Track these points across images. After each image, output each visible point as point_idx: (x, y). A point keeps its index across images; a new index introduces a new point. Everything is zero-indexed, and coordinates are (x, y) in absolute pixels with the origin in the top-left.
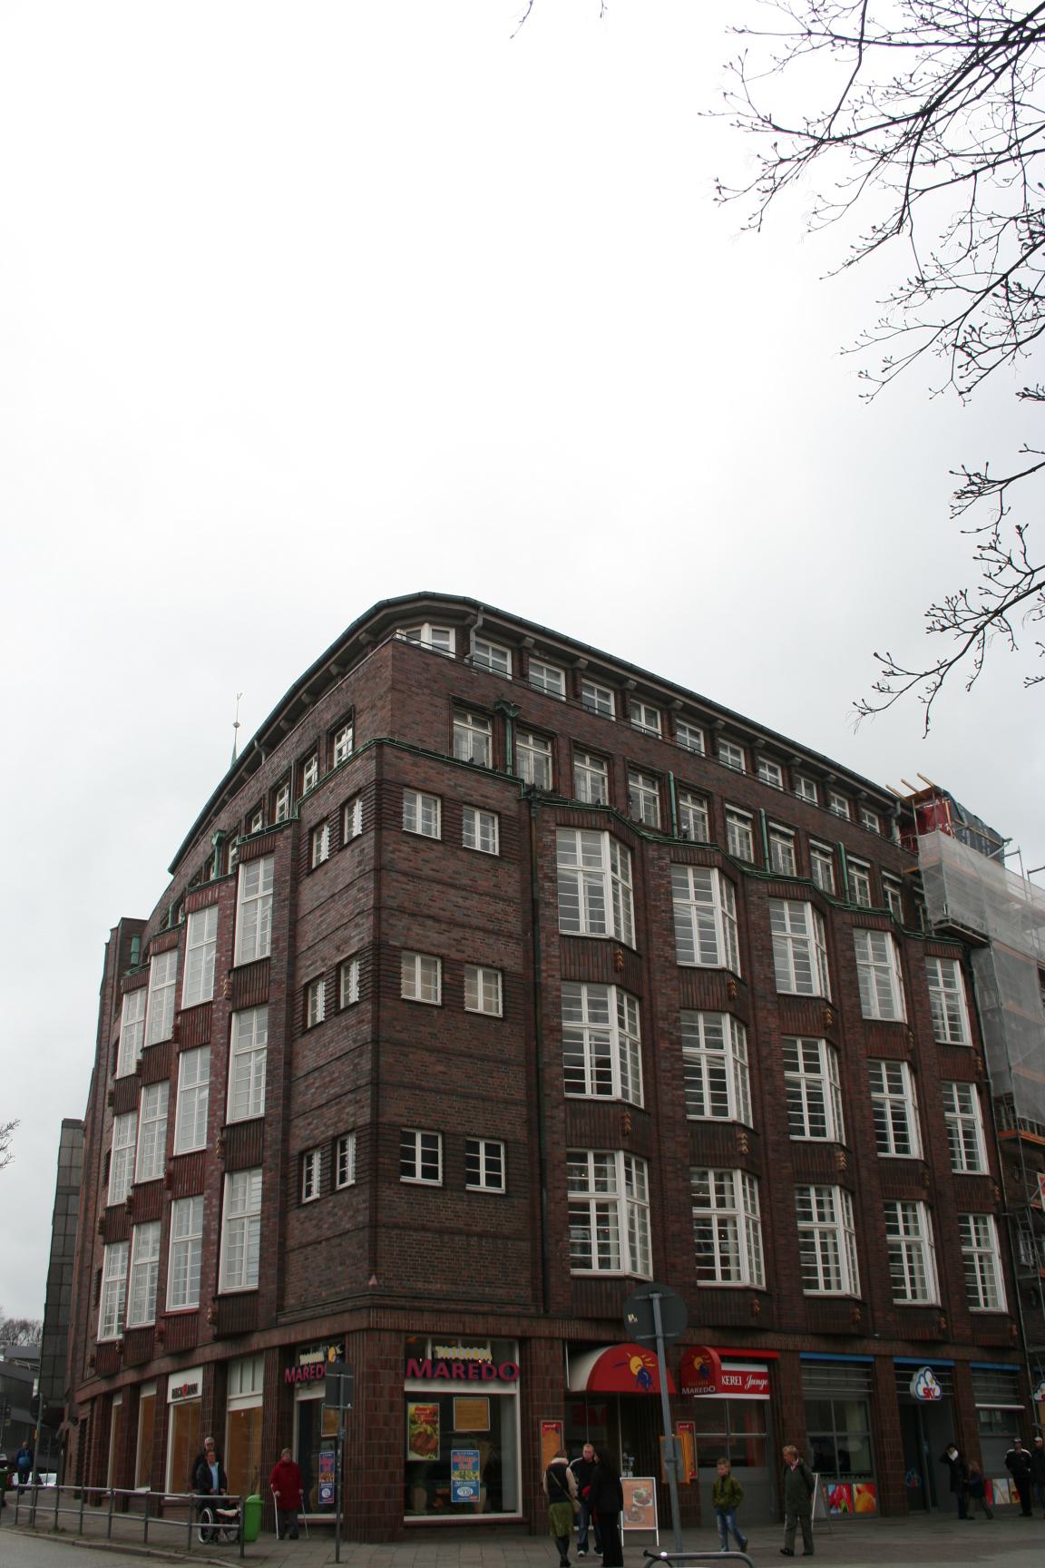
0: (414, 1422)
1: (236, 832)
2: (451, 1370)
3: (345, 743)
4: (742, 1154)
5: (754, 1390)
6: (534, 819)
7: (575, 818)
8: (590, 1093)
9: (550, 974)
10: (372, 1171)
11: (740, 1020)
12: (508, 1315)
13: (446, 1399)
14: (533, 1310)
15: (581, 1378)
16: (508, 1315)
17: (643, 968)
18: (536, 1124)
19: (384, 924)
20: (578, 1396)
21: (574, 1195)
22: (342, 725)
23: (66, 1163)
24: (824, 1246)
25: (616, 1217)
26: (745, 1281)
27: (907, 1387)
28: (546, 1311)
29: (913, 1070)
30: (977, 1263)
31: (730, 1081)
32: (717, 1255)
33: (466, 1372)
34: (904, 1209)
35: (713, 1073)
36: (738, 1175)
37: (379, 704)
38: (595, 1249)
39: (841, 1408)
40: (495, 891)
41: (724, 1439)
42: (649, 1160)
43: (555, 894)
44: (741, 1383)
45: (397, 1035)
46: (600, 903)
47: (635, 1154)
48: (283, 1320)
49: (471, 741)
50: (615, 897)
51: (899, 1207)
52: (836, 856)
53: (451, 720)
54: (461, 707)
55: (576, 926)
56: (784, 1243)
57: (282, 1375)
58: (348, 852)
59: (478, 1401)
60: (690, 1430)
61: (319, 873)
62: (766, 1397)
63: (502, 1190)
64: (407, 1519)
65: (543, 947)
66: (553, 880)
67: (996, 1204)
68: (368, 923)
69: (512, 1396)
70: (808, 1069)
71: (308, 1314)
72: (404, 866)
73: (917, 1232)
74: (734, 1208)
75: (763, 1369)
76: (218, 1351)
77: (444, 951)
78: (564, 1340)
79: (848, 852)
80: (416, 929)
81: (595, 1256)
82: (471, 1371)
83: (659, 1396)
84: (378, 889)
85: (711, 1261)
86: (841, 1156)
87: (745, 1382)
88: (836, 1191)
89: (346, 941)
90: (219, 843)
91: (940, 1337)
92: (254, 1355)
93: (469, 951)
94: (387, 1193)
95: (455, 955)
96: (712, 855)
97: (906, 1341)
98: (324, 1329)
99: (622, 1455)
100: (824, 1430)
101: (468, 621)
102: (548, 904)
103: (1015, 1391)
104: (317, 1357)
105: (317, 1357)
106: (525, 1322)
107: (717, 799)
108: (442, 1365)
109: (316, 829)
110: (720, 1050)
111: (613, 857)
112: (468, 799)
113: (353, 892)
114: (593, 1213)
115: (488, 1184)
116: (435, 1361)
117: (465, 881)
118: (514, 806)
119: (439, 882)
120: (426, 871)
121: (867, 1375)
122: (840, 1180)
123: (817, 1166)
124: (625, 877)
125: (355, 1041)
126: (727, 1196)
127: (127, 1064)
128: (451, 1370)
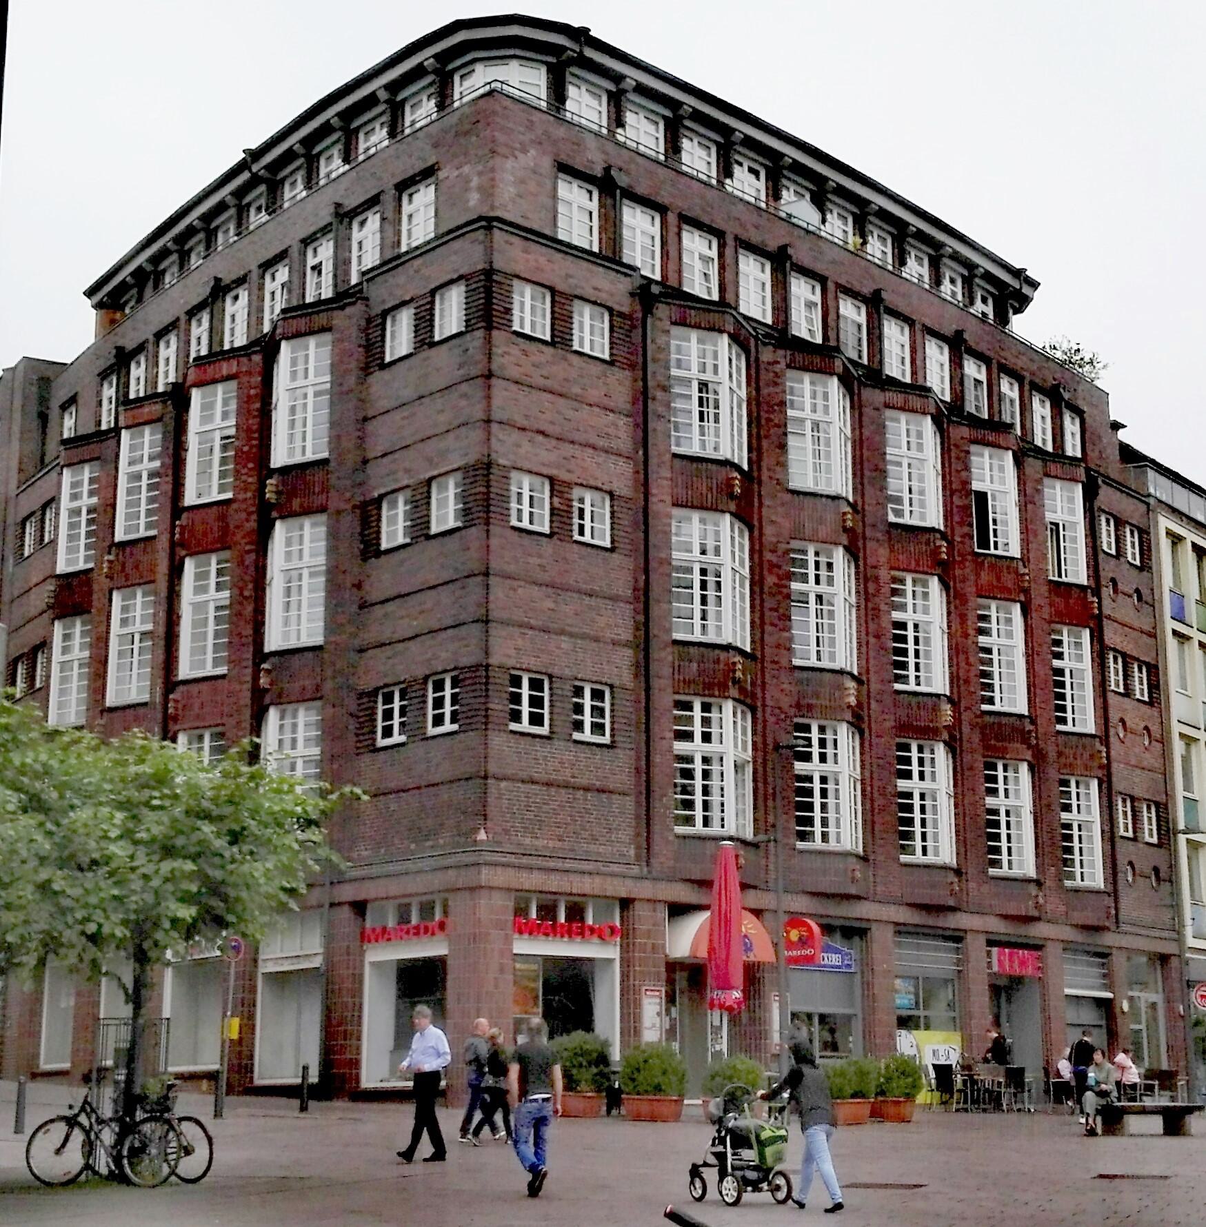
4: (849, 707)
19: (493, 440)
40: (606, 401)
43: (668, 406)
51: (1000, 767)
54: (565, 169)
66: (666, 389)
67: (1101, 767)
72: (514, 372)
77: (553, 472)
80: (526, 447)
86: (947, 709)
91: (1036, 914)
95: (564, 476)
96: (716, 314)
97: (909, 905)
102: (660, 416)
106: (629, 882)
112: (578, 292)
114: (817, 786)
117: (576, 390)
124: (739, 387)
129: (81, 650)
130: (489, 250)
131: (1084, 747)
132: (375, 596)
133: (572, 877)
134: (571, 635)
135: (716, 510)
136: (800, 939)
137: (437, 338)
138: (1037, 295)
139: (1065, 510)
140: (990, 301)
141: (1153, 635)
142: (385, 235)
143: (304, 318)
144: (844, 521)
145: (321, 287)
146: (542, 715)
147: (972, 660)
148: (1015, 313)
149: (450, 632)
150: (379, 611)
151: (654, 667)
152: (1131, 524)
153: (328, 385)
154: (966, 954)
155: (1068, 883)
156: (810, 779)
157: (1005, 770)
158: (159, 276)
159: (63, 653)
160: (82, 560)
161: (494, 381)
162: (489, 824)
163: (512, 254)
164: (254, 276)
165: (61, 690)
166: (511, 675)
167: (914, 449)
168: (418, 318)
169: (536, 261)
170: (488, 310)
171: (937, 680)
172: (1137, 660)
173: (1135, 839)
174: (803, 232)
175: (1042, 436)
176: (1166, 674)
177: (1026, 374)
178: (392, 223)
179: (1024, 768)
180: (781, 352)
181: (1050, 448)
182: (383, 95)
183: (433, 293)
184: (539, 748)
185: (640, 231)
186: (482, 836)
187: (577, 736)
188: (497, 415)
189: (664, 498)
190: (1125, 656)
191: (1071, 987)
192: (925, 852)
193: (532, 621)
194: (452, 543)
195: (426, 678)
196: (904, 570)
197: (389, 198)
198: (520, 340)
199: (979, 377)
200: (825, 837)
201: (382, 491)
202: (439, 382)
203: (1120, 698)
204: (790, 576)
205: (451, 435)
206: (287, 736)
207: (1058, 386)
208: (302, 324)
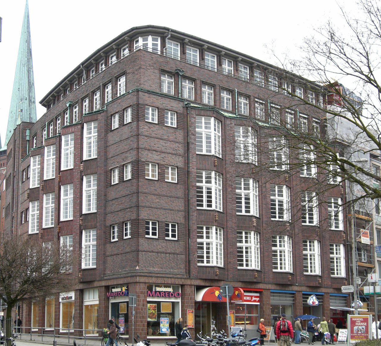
0: (149, 310)
4: (254, 226)
5: (255, 301)
6: (188, 113)
8: (205, 207)
9: (193, 170)
10: (135, 234)
12: (178, 278)
13: (159, 303)
14: (185, 276)
15: (200, 297)
16: (178, 278)
18: (187, 217)
19: (140, 154)
20: (199, 302)
24: (281, 256)
25: (213, 248)
27: (306, 301)
28: (190, 277)
31: (251, 201)
32: (244, 259)
33: (165, 295)
35: (246, 199)
36: (252, 233)
37: (136, 73)
38: (205, 257)
39: (284, 308)
40: (175, 140)
41: (244, 316)
42: (223, 228)
43: (195, 140)
44: (250, 299)
45: (144, 191)
46: (210, 143)
48: (105, 278)
49: (167, 84)
52: (295, 115)
53: (160, 77)
54: (163, 72)
55: (202, 151)
56: (268, 256)
57: (106, 295)
59: (168, 303)
60: (233, 313)
62: (258, 303)
63: (176, 239)
64: (148, 337)
65: (191, 158)
66: (194, 135)
67: (344, 240)
69: (178, 302)
70: (279, 195)
71: (114, 276)
72: (146, 134)
73: (314, 251)
74: (251, 244)
75: (258, 295)
76: (81, 286)
77: (159, 162)
78: (195, 286)
79: (300, 113)
80: (150, 155)
82: (166, 294)
83: (226, 303)
85: (242, 261)
87: (251, 299)
89: (126, 157)
90: (70, 106)
91: (319, 285)
92: (94, 288)
93: (167, 161)
94: (141, 241)
95: (162, 163)
96: (214, 111)
97: (275, 284)
98: (121, 282)
99: (212, 320)
100: (346, 306)
101: (165, 35)
102: (193, 143)
103: (346, 303)
104: (119, 290)
105: (119, 290)
106: (183, 280)
107: (252, 98)
108: (158, 293)
109: (113, 115)
111: (215, 125)
112: (166, 108)
114: (244, 250)
115: (172, 237)
116: (156, 292)
117: (166, 137)
118: (182, 109)
120: (153, 135)
121: (293, 297)
123: (281, 229)
124: (219, 132)
125: (130, 192)
126: (249, 239)
129: (52, 204)
130: (138, 98)
131: (338, 234)
132: (109, 199)
137: (125, 123)
143: (92, 116)
145: (97, 106)
149: (129, 209)
150: (111, 203)
151: (191, 217)
154: (296, 298)
158: (59, 97)
159: (32, 212)
160: (36, 184)
161: (139, 136)
162: (140, 264)
164: (80, 101)
165: (46, 216)
168: (120, 117)
169: (153, 100)
170: (139, 116)
178: (114, 88)
179: (316, 242)
183: (124, 110)
184: (155, 243)
186: (137, 268)
188: (141, 146)
191: (332, 306)
194: (129, 184)
195: (123, 222)
197: (114, 80)
198: (147, 124)
200: (247, 265)
201: (111, 168)
204: (236, 188)
205: (129, 152)
206: (88, 238)
208: (90, 118)
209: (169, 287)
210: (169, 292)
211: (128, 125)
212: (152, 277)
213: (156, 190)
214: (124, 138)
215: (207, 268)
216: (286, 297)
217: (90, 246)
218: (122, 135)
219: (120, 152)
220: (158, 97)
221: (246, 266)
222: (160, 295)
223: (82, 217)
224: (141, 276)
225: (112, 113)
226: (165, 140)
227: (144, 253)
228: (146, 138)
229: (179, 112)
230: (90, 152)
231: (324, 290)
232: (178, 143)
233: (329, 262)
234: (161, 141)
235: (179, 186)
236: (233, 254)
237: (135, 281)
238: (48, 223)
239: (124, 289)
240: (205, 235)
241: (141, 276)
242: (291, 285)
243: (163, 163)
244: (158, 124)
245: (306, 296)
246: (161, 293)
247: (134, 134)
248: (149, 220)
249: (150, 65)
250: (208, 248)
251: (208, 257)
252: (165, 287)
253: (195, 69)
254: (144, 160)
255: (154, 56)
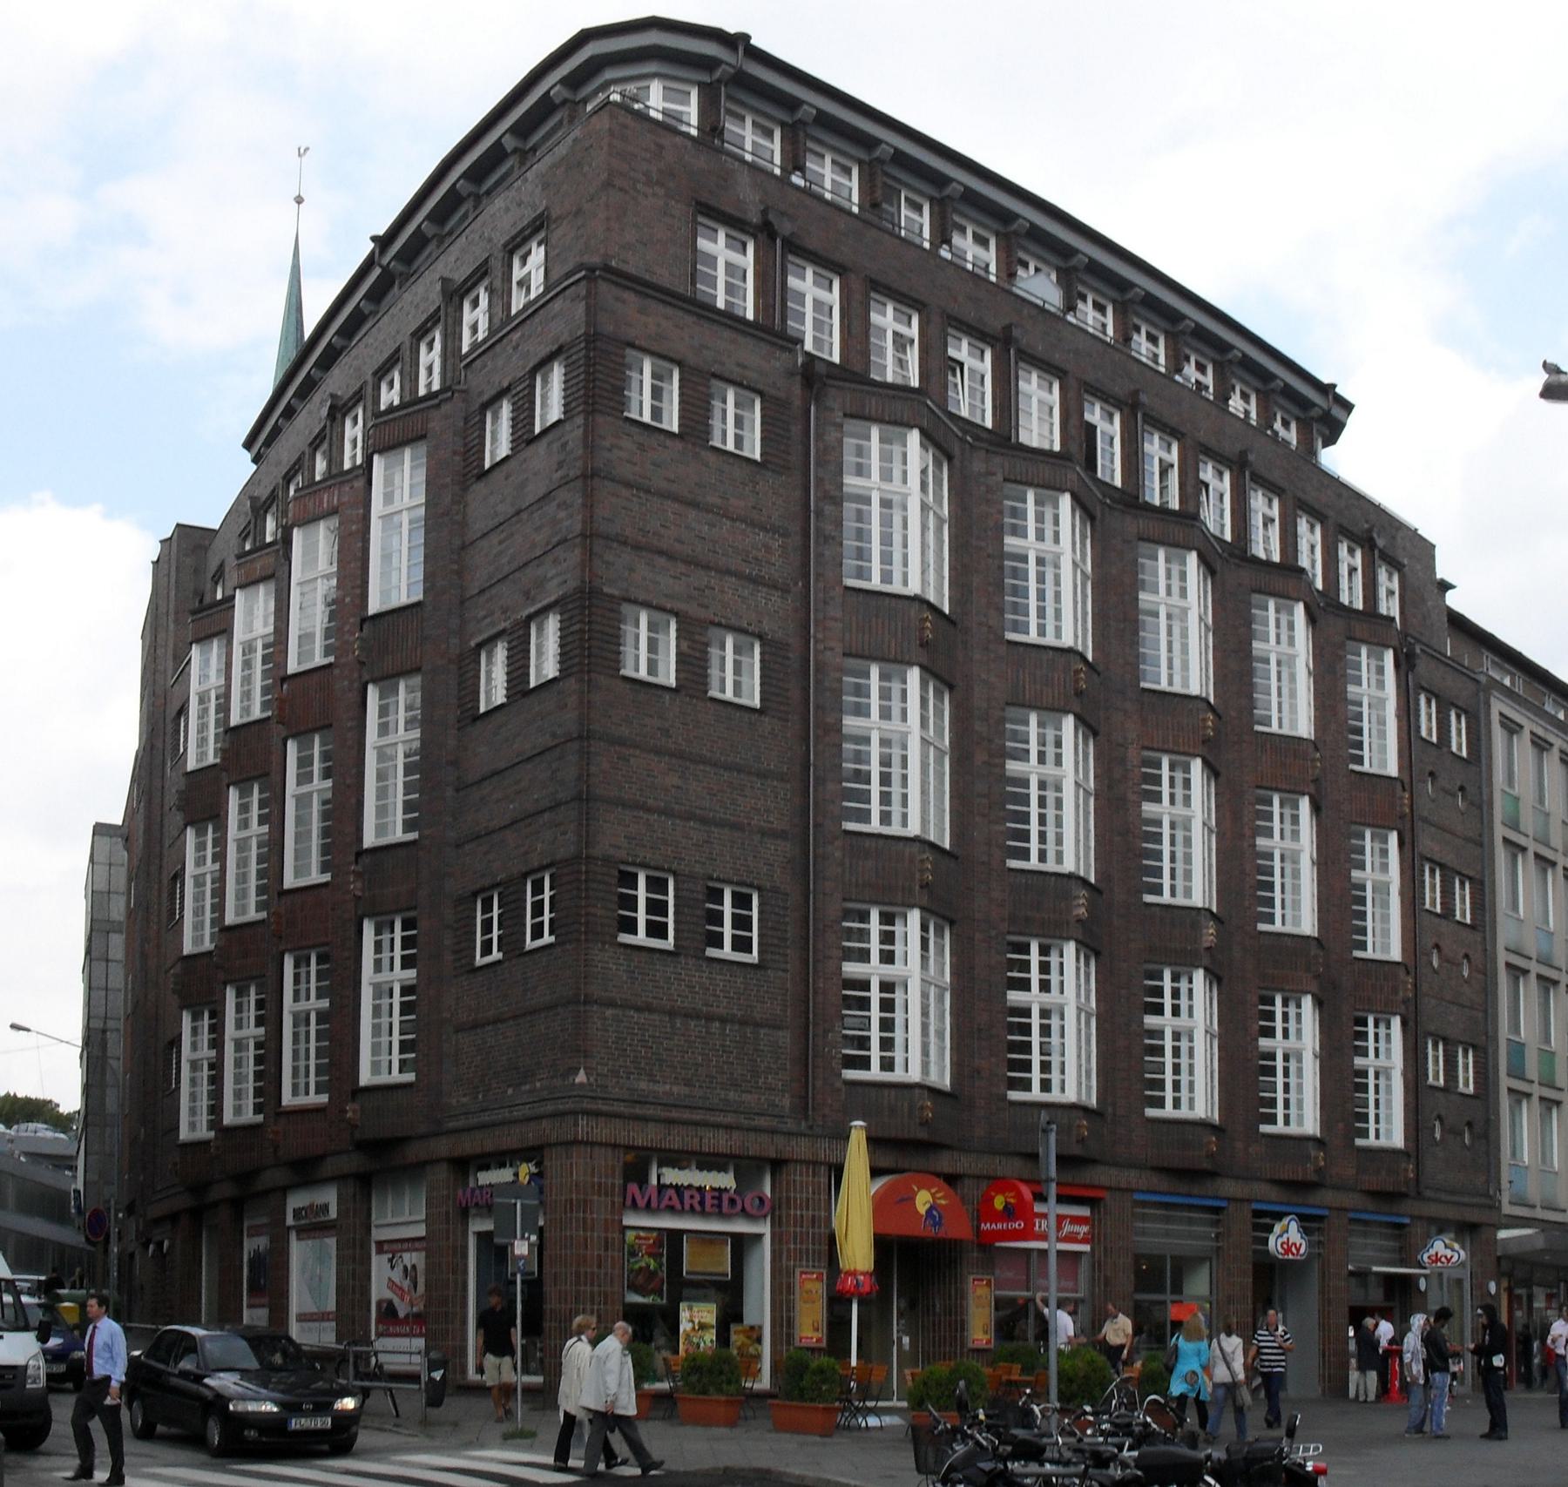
1: (358, 397)
2: (679, 1200)
3: (533, 267)
7: (873, 405)
11: (1088, 726)
12: (756, 1130)
16: (756, 1130)
17: (961, 645)
21: (851, 969)
22: (526, 240)
23: (102, 886)
26: (1071, 1096)
29: (1316, 808)
30: (1371, 1081)
32: (1036, 1058)
33: (702, 1203)
34: (1285, 1003)
36: (1070, 948)
47: (936, 914)
48: (451, 1125)
49: (728, 267)
50: (924, 528)
51: (1278, 1000)
58: (541, 447)
61: (498, 475)
62: (1086, 1248)
63: (754, 957)
67: (1405, 1001)
68: (574, 556)
69: (759, 1237)
73: (1192, 1014)
74: (1063, 994)
75: (1084, 1211)
81: (875, 1053)
84: (589, 506)
85: (1027, 1066)
88: (1199, 976)
89: (540, 583)
97: (1153, 1169)
100: (1402, 1263)
104: (503, 1176)
106: (780, 1140)
108: (672, 1192)
110: (1057, 768)
112: (715, 368)
113: (550, 508)
114: (875, 995)
115: (734, 948)
116: (661, 1187)
117: (712, 499)
119: (676, 498)
122: (1206, 961)
125: (554, 735)
127: (199, 748)
128: (679, 1200)
133: (701, 1131)
134: (704, 821)
135: (901, 662)
136: (1005, 1207)
138: (1353, 422)
139: (1373, 682)
140: (1293, 426)
141: (1481, 845)
142: (494, 311)
144: (1077, 681)
146: (636, 919)
147: (1248, 868)
148: (1325, 445)
152: (1457, 707)
153: (423, 510)
155: (1359, 1142)
156: (865, 985)
157: (1376, 1026)
163: (630, 314)
166: (620, 872)
167: (1178, 597)
169: (659, 325)
170: (598, 393)
171: (1199, 891)
172: (1459, 873)
173: (1444, 1090)
174: (1034, 312)
175: (1352, 594)
176: (1493, 892)
177: (1331, 513)
179: (1307, 1002)
180: (997, 460)
181: (1359, 605)
182: (510, 143)
185: (815, 301)
186: (581, 1077)
187: (712, 952)
189: (832, 644)
190: (1442, 866)
192: (1177, 1103)
193: (650, 802)
196: (1158, 750)
198: (634, 430)
199: (1269, 512)
201: (479, 639)
202: (536, 489)
203: (1437, 920)
205: (550, 557)
207: (1370, 530)
209: (722, 1168)
210: (719, 1190)
211: (550, 436)
212: (645, 1119)
213: (666, 732)
214: (531, 499)
215: (886, 1092)
216: (1190, 1221)
217: (391, 990)
218: (523, 485)
219: (515, 565)
220: (680, 313)
221: (1043, 1090)
222: (682, 1203)
223: (366, 860)
224: (598, 1114)
225: (486, 397)
226: (708, 511)
227: (609, 1012)
228: (625, 492)
229: (773, 392)
230: (395, 579)
231: (1328, 1197)
232: (766, 530)
233: (1351, 1087)
234: (692, 514)
235: (767, 723)
236: (990, 1030)
237: (570, 1137)
238: (242, 908)
239: (525, 1170)
240: (875, 946)
241: (598, 1114)
242: (1212, 1175)
243: (702, 614)
244: (679, 437)
245: (1264, 1221)
246: (687, 1194)
247: (572, 474)
248: (634, 864)
249: (647, 174)
250: (887, 1005)
251: (887, 1044)
252: (701, 1168)
253: (842, 223)
254: (616, 593)
255: (667, 140)
